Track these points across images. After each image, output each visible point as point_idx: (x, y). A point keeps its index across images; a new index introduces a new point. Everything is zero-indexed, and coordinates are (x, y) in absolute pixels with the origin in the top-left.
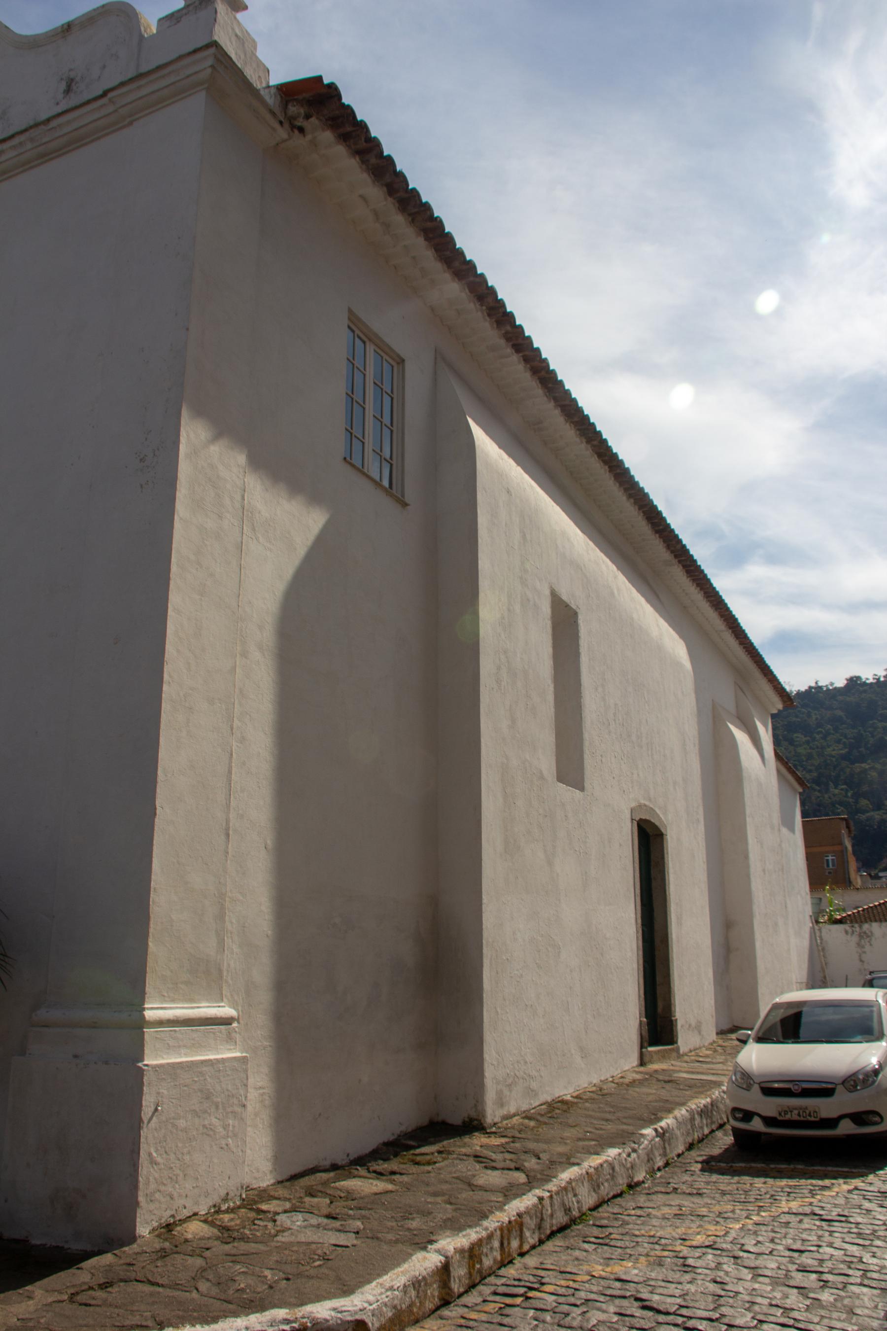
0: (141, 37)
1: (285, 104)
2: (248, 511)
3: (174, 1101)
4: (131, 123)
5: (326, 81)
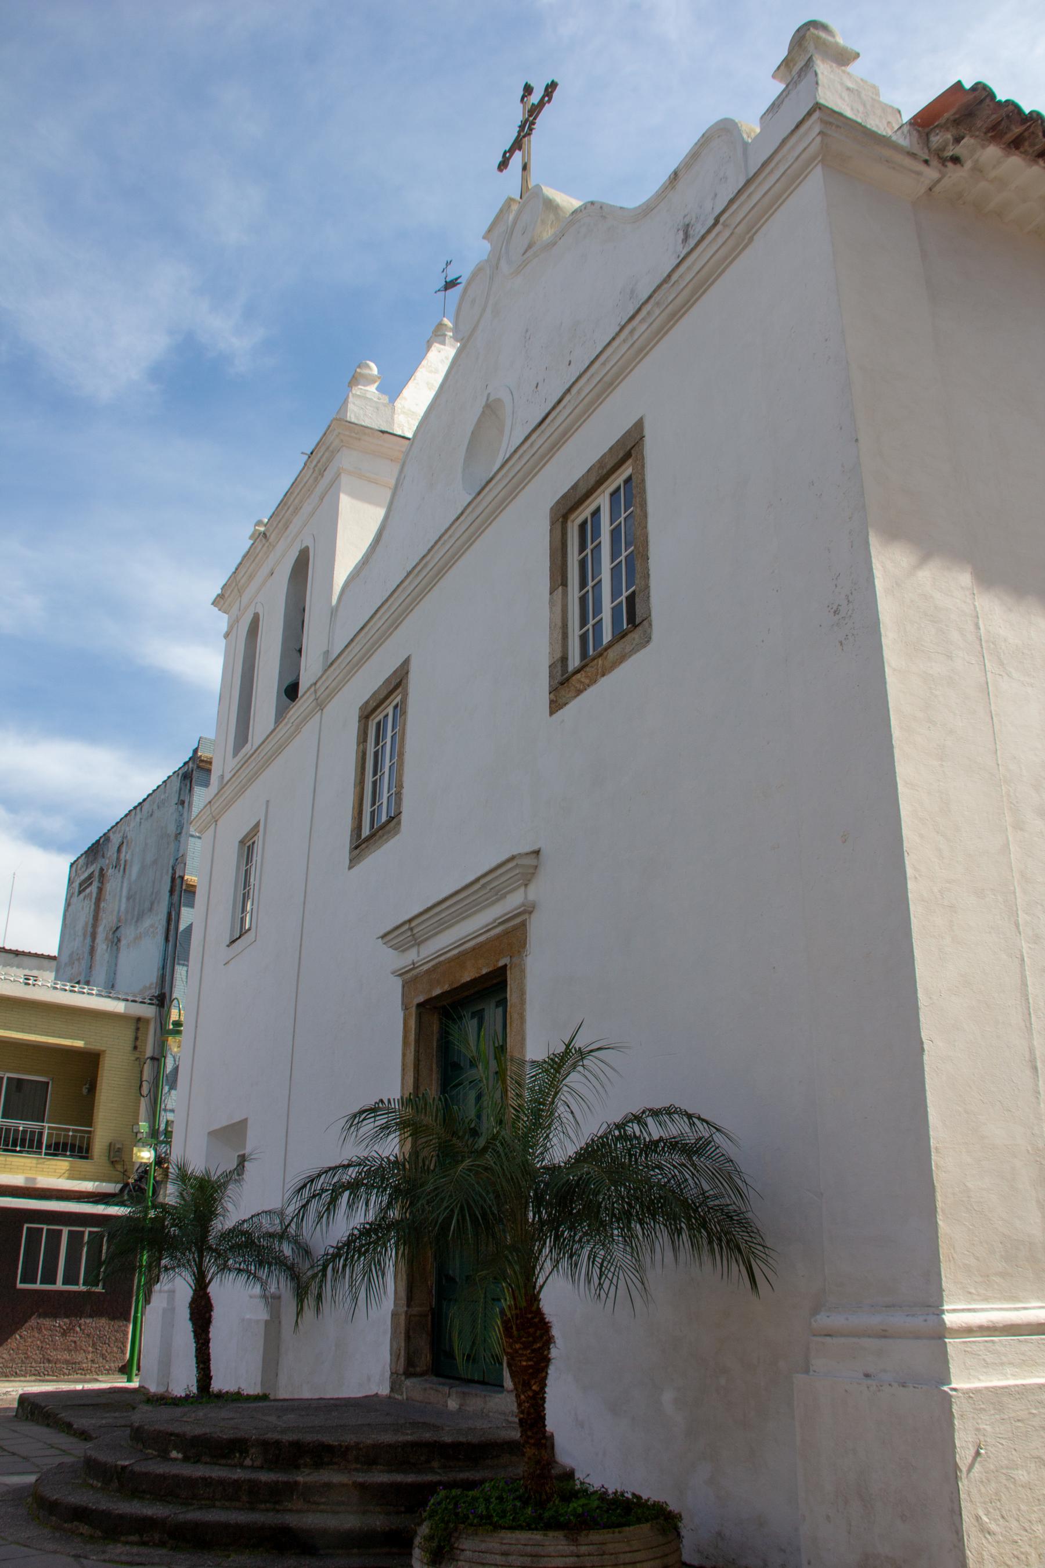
0: (745, 144)
1: (925, 138)
2: (987, 642)
3: (1003, 1442)
4: (751, 239)
5: (968, 85)
